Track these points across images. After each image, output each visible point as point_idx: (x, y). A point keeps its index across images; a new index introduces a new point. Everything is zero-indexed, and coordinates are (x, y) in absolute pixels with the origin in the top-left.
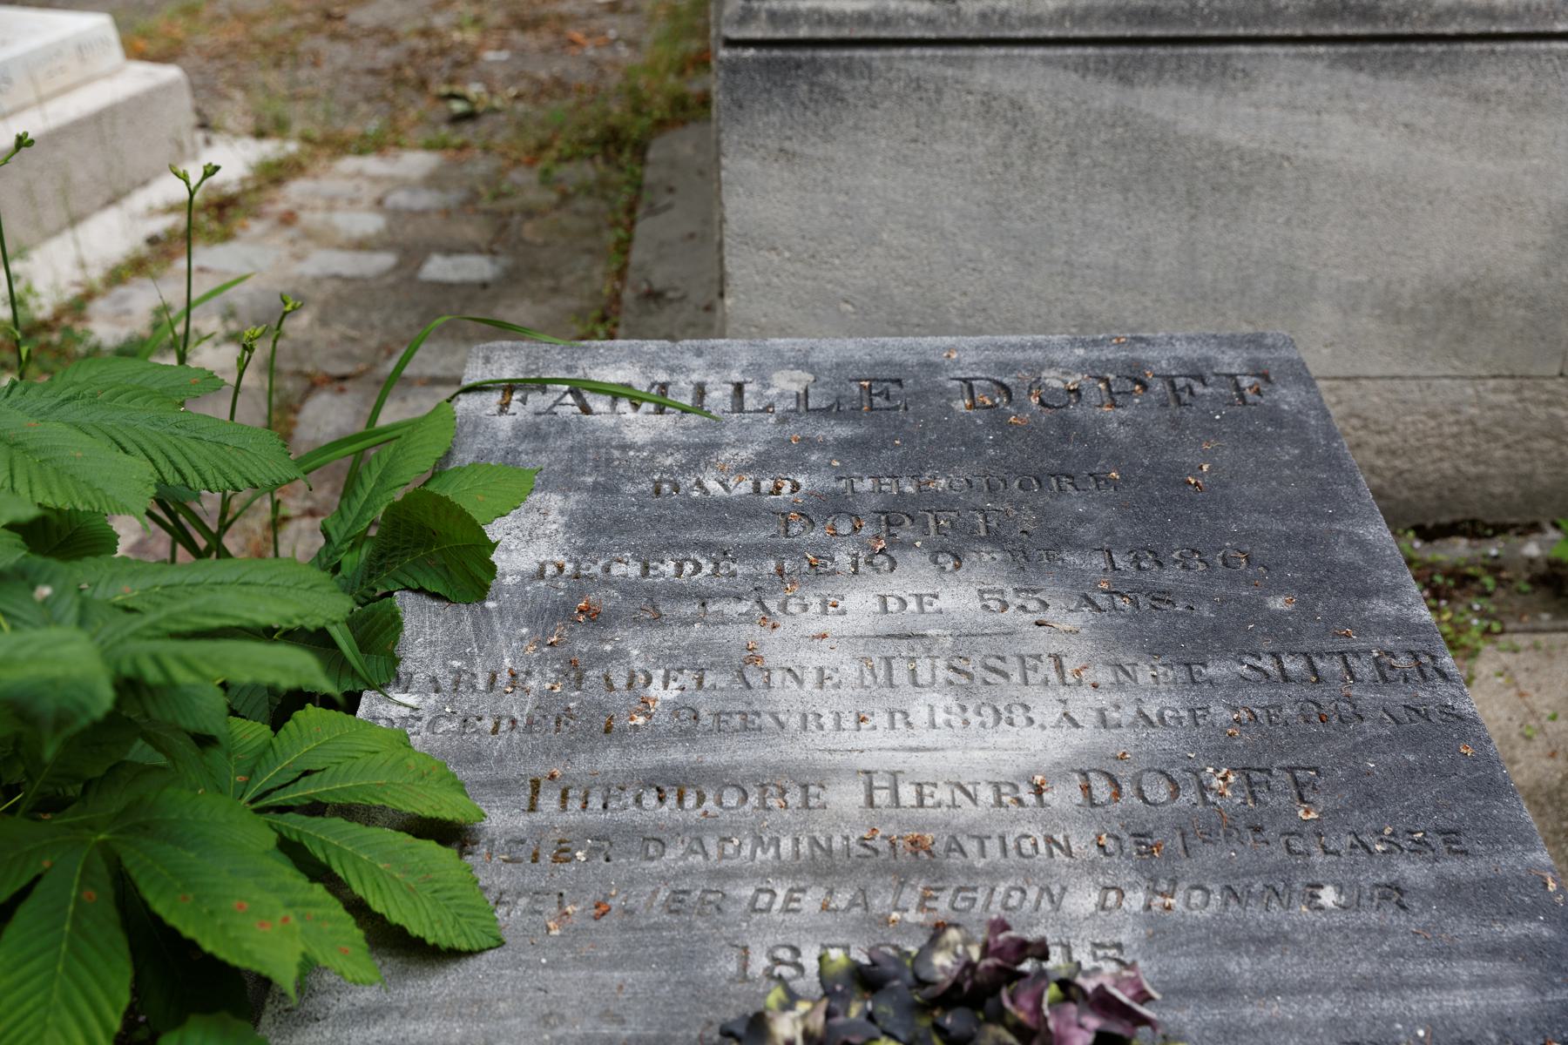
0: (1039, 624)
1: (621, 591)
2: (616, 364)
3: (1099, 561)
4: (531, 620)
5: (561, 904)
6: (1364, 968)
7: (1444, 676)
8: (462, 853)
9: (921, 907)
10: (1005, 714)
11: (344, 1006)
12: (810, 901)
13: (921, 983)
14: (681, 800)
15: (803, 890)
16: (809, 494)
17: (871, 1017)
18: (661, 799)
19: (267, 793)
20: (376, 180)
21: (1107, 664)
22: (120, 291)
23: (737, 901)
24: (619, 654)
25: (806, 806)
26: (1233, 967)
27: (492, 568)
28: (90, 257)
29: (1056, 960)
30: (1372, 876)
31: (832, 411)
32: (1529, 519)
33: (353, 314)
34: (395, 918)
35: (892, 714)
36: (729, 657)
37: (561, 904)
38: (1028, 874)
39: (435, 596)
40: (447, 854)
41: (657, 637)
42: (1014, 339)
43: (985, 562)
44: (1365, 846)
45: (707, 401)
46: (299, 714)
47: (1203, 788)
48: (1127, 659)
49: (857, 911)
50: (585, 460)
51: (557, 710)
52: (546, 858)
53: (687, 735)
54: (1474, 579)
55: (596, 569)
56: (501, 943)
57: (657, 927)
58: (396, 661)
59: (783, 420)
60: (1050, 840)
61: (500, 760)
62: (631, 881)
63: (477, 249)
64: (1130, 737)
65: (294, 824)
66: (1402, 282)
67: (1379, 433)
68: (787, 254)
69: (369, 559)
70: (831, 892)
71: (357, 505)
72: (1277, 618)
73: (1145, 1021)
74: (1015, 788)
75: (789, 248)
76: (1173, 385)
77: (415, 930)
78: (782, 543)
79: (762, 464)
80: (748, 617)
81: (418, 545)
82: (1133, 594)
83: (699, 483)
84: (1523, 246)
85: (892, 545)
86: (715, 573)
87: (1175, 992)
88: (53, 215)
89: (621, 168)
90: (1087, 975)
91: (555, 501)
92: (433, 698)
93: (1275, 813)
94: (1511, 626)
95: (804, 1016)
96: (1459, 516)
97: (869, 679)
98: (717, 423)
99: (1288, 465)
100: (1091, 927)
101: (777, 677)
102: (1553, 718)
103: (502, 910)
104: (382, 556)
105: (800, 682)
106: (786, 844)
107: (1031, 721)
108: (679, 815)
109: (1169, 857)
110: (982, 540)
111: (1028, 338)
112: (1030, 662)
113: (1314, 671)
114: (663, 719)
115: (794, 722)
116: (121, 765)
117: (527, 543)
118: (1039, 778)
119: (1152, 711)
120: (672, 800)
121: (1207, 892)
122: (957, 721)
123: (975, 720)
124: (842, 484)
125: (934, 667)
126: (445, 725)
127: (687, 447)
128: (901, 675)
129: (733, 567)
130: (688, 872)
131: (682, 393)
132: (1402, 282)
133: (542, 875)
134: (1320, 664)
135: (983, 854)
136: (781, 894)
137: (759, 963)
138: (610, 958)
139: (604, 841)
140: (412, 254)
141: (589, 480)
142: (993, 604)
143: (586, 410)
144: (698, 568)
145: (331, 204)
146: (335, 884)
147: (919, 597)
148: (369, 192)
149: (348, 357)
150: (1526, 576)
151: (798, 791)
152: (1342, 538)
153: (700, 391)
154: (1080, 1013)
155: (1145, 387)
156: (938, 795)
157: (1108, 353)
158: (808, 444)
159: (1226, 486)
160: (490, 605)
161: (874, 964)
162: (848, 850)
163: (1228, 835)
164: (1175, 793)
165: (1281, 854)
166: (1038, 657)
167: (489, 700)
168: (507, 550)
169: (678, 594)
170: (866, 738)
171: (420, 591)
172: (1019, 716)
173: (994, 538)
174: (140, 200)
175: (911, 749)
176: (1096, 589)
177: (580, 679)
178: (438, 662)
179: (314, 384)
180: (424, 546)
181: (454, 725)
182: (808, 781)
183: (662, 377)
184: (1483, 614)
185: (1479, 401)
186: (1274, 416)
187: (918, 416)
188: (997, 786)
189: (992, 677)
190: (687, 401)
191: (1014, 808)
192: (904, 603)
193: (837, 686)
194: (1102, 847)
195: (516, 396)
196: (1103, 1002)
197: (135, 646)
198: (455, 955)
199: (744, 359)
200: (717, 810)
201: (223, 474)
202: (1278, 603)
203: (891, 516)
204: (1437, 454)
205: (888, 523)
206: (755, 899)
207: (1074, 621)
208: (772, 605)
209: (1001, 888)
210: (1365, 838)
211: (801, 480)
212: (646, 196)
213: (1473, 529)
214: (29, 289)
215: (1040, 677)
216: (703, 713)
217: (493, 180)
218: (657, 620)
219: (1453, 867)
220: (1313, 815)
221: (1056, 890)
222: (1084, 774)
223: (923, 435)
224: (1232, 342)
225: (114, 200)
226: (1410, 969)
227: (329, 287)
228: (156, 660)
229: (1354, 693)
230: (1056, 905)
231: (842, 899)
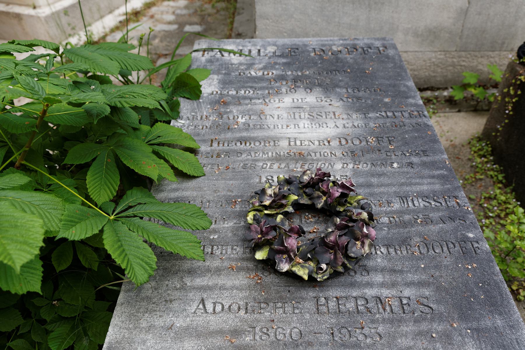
0: (330, 105)
1: (232, 97)
2: (230, 45)
3: (344, 90)
4: (210, 104)
5: (218, 167)
6: (403, 181)
7: (425, 116)
8: (195, 155)
9: (301, 167)
10: (321, 125)
11: (169, 188)
12: (276, 166)
13: (301, 183)
14: (246, 144)
15: (274, 164)
16: (276, 75)
17: (289, 190)
18: (241, 144)
19: (150, 141)
20: (172, 7)
21: (346, 114)
22: (113, 34)
23: (258, 166)
24: (231, 112)
25: (275, 145)
26: (373, 180)
27: (201, 92)
28: (106, 26)
29: (332, 178)
30: (405, 161)
31: (282, 56)
32: (445, 86)
33: (168, 40)
34: (180, 168)
35: (295, 125)
36: (257, 112)
37: (218, 167)
38: (326, 160)
39: (188, 98)
40: (192, 155)
41: (240, 108)
42: (325, 39)
43: (318, 90)
44: (404, 154)
45: (252, 53)
46: (157, 124)
47: (367, 142)
48: (350, 113)
49: (286, 168)
50: (222, 68)
51: (217, 124)
52: (215, 157)
53: (247, 130)
54: (431, 100)
55: (226, 92)
56: (205, 175)
57: (240, 172)
58: (179, 113)
59: (270, 58)
60: (331, 153)
61: (204, 135)
62: (234, 162)
63: (196, 24)
64: (351, 130)
65: (156, 148)
66: (419, 27)
67: (412, 65)
68: (271, 21)
69: (172, 90)
70: (280, 164)
71: (169, 78)
72: (386, 103)
73: (352, 190)
74: (323, 141)
75: (271, 19)
76: (363, 50)
77: (185, 171)
78: (269, 86)
79: (265, 68)
80: (261, 103)
81: (184, 87)
82: (353, 97)
83: (250, 73)
84: (449, 18)
85: (295, 87)
86: (253, 93)
87: (359, 186)
88: (97, 16)
89: (231, 4)
90: (339, 181)
91: (215, 77)
92: (188, 121)
93: (384, 147)
94: (439, 111)
95: (274, 189)
96: (429, 86)
97: (289, 117)
98: (254, 59)
99: (391, 68)
100: (340, 171)
101: (268, 117)
102: (448, 132)
103: (205, 168)
104: (175, 89)
105: (273, 118)
106: (270, 154)
107: (327, 127)
108: (245, 147)
109: (359, 156)
110: (317, 86)
111: (329, 39)
112: (328, 113)
113: (394, 115)
114: (241, 126)
115: (272, 127)
116: (115, 133)
117: (209, 87)
118: (329, 139)
119: (356, 124)
120: (243, 144)
121: (367, 164)
122: (310, 127)
123: (314, 126)
124: (284, 73)
125: (305, 115)
126: (191, 127)
127: (247, 64)
128: (297, 116)
129: (258, 92)
130: (247, 160)
131: (245, 52)
132: (419, 27)
133: (214, 160)
134: (396, 114)
135: (316, 156)
136: (269, 165)
137: (264, 179)
138: (230, 178)
139: (228, 153)
140: (181, 25)
141: (224, 72)
142: (319, 100)
143: (223, 56)
144: (249, 92)
145: (162, 13)
146: (167, 161)
147: (302, 99)
148: (171, 10)
149: (167, 50)
150: (443, 100)
151: (273, 142)
152: (402, 85)
153: (250, 51)
154: (337, 188)
155: (357, 50)
156: (305, 143)
157: (348, 42)
158: (276, 63)
159: (375, 73)
160: (201, 100)
161: (290, 178)
162: (284, 155)
163: (373, 152)
164: (361, 142)
165: (385, 156)
166: (329, 112)
167: (201, 122)
168: (204, 88)
169: (245, 98)
170: (289, 130)
171: (184, 97)
172: (325, 125)
173: (320, 85)
174: (117, 12)
175: (299, 133)
176: (343, 97)
177: (222, 117)
178: (189, 113)
179: (160, 56)
180: (186, 87)
181: (193, 128)
182: (275, 140)
183: (241, 48)
184: (433, 109)
185: (436, 57)
186: (388, 57)
187: (302, 57)
188: (319, 141)
189: (318, 117)
190: (247, 53)
191: (323, 146)
192: (298, 100)
193: (282, 119)
194: (343, 154)
195: (206, 53)
196: (343, 186)
197: (114, 99)
198: (194, 177)
199: (261, 44)
200: (254, 146)
201: (136, 67)
202: (387, 100)
203: (295, 80)
204: (425, 70)
205: (295, 82)
206: (263, 166)
207: (338, 104)
208: (267, 100)
209: (320, 163)
210: (404, 152)
211: (274, 72)
212: (237, 10)
213: (432, 89)
214: (92, 34)
215: (330, 117)
216: (251, 125)
217: (201, 7)
218: (240, 104)
219: (425, 159)
220: (393, 147)
221: (332, 164)
222: (340, 138)
223: (303, 61)
224: (378, 39)
225: (111, 12)
226: (413, 181)
227: (162, 33)
228: (120, 102)
229: (404, 120)
230: (332, 167)
231: (283, 166)
